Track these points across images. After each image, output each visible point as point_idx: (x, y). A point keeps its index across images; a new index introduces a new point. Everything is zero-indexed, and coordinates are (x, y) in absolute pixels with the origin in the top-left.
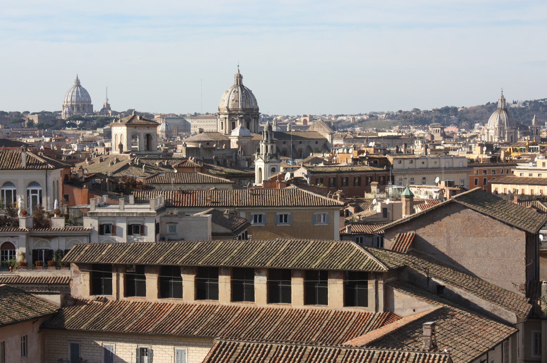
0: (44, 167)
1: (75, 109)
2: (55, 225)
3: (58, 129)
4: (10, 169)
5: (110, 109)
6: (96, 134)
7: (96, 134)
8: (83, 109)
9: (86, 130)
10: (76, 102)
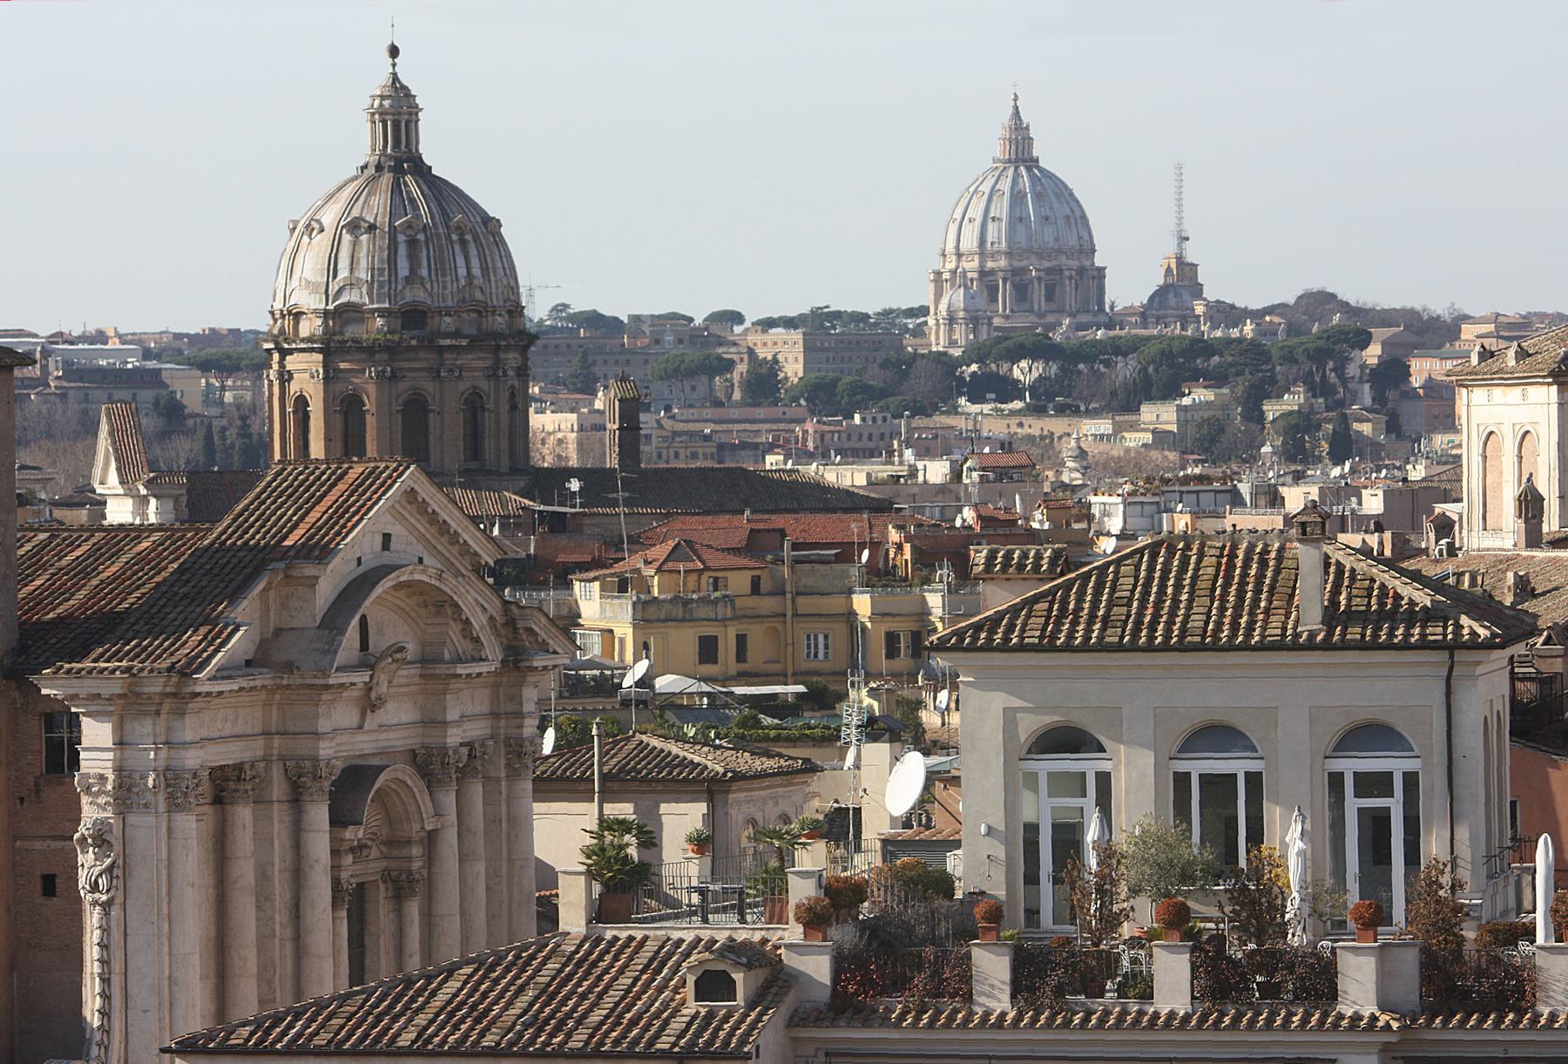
0: (1435, 632)
1: (1004, 292)
2: (1557, 991)
3: (921, 410)
4: (1231, 648)
5: (1197, 290)
6: (1134, 440)
7: (1134, 440)
8: (1050, 297)
9: (1076, 412)
10: (1009, 254)
